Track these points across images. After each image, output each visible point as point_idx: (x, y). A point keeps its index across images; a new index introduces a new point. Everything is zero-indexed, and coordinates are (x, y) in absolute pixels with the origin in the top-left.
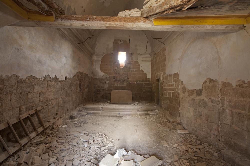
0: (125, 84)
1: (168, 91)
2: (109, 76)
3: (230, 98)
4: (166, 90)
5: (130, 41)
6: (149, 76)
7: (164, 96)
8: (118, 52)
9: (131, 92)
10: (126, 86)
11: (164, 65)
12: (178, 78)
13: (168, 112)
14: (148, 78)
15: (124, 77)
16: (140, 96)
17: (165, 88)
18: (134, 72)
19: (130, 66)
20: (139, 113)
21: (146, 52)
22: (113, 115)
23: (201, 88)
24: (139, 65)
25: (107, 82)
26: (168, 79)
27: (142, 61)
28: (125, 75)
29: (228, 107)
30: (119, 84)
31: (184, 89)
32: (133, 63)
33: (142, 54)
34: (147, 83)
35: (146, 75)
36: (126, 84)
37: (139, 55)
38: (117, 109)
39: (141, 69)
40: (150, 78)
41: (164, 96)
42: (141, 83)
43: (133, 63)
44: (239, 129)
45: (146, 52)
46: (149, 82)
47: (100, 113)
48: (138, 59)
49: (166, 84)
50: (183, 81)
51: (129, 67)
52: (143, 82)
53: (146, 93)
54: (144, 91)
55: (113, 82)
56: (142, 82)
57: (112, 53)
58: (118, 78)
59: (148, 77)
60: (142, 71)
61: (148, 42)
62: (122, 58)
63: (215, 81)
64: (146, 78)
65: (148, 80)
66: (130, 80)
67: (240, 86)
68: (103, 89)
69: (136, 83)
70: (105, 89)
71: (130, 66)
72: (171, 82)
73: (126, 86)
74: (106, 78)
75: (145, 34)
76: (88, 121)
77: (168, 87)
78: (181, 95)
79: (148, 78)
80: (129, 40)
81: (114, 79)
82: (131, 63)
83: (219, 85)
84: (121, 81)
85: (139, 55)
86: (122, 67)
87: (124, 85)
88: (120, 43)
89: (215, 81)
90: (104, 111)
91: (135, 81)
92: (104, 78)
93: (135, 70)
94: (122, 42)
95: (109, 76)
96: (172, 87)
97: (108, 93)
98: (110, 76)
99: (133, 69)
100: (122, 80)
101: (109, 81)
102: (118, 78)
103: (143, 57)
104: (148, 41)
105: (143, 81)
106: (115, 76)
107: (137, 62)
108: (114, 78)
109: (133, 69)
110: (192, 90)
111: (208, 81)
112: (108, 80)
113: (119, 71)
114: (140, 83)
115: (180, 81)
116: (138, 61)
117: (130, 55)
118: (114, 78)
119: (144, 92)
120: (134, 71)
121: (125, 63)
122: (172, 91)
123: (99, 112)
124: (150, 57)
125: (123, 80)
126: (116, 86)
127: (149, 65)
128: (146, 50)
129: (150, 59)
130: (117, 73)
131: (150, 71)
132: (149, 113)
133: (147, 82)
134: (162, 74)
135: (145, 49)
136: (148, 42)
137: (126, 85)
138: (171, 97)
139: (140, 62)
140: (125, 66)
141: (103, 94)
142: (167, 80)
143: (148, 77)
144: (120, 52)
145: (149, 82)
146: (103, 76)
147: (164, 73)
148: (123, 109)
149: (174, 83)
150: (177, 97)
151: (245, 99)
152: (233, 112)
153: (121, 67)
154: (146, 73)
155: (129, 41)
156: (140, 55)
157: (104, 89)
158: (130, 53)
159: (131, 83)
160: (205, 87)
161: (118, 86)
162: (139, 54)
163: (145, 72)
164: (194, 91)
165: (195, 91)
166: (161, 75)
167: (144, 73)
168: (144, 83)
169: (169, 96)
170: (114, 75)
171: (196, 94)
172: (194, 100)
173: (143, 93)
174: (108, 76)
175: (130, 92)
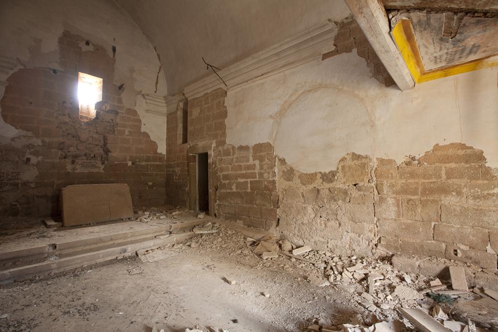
0: (100, 168)
1: (237, 179)
2: (40, 141)
3: (393, 181)
4: (226, 177)
5: (117, 52)
6: (162, 149)
7: (223, 191)
8: (77, 76)
9: (128, 188)
10: (103, 171)
11: (221, 127)
12: (268, 154)
13: (241, 222)
14: (159, 153)
15: (91, 146)
16: (140, 197)
17: (224, 173)
18: (125, 136)
19: (112, 120)
20: (175, 237)
21: (156, 92)
22: (101, 260)
23: (334, 169)
24: (140, 121)
25: (34, 160)
26: (236, 156)
27: (147, 111)
28: (97, 143)
29: (390, 193)
30: (78, 167)
31: (289, 174)
32: (124, 112)
33: (147, 95)
34: (157, 165)
35: (154, 145)
36: (102, 167)
37: (139, 96)
38: (112, 240)
39: (143, 129)
40: (164, 153)
41: (223, 191)
42: (144, 163)
43: (124, 112)
44: (409, 221)
45: (156, 92)
46: (161, 163)
47: (54, 266)
48: (135, 105)
49: (230, 166)
50: (284, 158)
51: (109, 122)
52: (149, 163)
53: (155, 188)
54: (150, 184)
55: (58, 160)
56: (146, 161)
57: (55, 71)
58: (72, 149)
59: (159, 151)
60: (146, 135)
61: (160, 70)
62: (88, 92)
63: (364, 158)
64: (156, 152)
65: (159, 158)
66: (115, 155)
67: (408, 164)
68: (16, 185)
69: (130, 163)
70: (25, 184)
71: (112, 120)
72: (248, 161)
73: (103, 171)
74: (29, 146)
75: (155, 48)
76: (28, 314)
77: (237, 171)
78: (281, 184)
79: (161, 154)
80: (114, 49)
81: (60, 152)
82: (117, 113)
83: (374, 163)
84: (84, 157)
85: (138, 94)
86: (86, 118)
87: (95, 170)
88: (85, 48)
89: (364, 158)
90: (61, 256)
91: (128, 159)
92: (18, 144)
93: (129, 131)
94: (90, 48)
95: (43, 141)
96: (253, 171)
97: (38, 197)
98: (47, 140)
99: (122, 129)
100: (85, 155)
101: (40, 158)
102: (72, 149)
103: (148, 101)
104: (160, 67)
105: (148, 159)
106: (63, 143)
107: (135, 113)
108: (61, 149)
109: (122, 129)
110: (312, 174)
111: (349, 157)
112: (36, 154)
113: (75, 128)
114: (141, 164)
115: (277, 158)
116: (136, 108)
117: (113, 89)
118: (61, 146)
119: (151, 187)
120: (125, 133)
121: (96, 108)
122: (252, 180)
123: (44, 264)
124: (165, 105)
125: (90, 154)
126: (69, 173)
127: (162, 121)
128: (155, 87)
129: (165, 110)
130: (69, 134)
131: (165, 138)
132: (197, 231)
133: (157, 163)
134: (213, 146)
135: (155, 85)
136: (160, 70)
137: (104, 169)
138: (249, 190)
139: (141, 112)
140: (97, 118)
141: (17, 201)
142: (230, 157)
143: (159, 151)
144: (82, 75)
145: (161, 163)
146: (13, 139)
147: (223, 143)
148: (129, 236)
149: (257, 162)
150: (269, 190)
151: (416, 180)
152: (399, 200)
153: (82, 117)
154: (156, 142)
155: (112, 52)
156: (143, 95)
157: (20, 181)
158: (116, 84)
159: (116, 165)
160: (343, 167)
161: (76, 171)
162: (140, 93)
163: (152, 139)
164: (316, 176)
165: (319, 176)
166: (211, 146)
167: (151, 141)
168: (151, 166)
169: (239, 190)
170: (61, 140)
171: (321, 180)
172: (318, 191)
173: (147, 188)
174: (38, 142)
175: (125, 188)
